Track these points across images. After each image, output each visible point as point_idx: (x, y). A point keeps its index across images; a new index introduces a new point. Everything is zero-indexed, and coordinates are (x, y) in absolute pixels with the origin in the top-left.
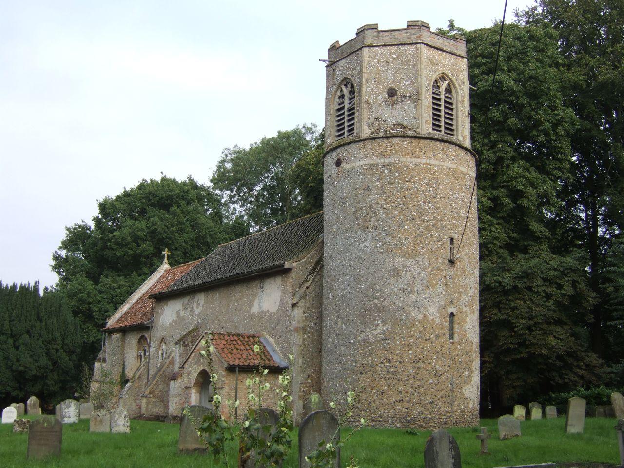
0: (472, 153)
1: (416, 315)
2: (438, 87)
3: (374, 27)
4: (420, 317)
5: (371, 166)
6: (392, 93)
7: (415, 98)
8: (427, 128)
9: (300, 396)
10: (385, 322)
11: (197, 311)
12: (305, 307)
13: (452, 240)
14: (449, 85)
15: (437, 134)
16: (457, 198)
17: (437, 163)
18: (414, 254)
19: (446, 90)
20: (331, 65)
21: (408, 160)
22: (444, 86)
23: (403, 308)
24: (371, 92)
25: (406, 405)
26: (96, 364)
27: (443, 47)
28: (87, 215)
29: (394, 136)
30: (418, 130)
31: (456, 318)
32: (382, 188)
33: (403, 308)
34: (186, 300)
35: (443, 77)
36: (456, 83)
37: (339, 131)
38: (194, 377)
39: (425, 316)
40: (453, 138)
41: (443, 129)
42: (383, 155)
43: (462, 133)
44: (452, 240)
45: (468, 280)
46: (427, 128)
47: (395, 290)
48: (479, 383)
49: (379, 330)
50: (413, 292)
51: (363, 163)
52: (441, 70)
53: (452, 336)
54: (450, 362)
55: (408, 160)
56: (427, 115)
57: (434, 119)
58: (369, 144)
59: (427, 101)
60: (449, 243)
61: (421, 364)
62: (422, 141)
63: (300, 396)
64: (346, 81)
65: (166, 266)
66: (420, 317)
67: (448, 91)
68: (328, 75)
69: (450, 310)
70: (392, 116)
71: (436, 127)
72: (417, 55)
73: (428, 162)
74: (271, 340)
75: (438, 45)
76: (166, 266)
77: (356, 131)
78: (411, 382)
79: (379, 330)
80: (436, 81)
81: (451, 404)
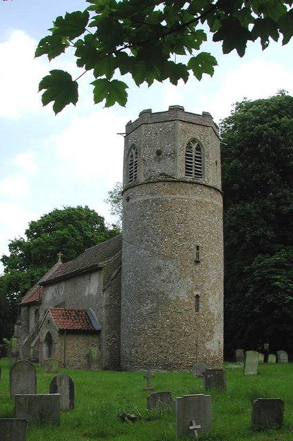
0: (221, 192)
1: (172, 296)
2: (191, 147)
3: (182, 109)
4: (174, 298)
5: (147, 201)
6: (159, 153)
7: (173, 155)
8: (181, 175)
9: (107, 349)
10: (152, 302)
11: (62, 293)
12: (111, 292)
13: (198, 248)
14: (198, 145)
15: (189, 179)
16: (202, 220)
17: (187, 197)
18: (170, 257)
19: (196, 148)
20: (127, 136)
21: (168, 197)
22: (194, 146)
23: (163, 292)
24: (147, 153)
25: (164, 354)
26: (15, 326)
27: (192, 121)
28: (20, 233)
29: (160, 181)
30: (174, 177)
31: (200, 298)
32: (152, 215)
33: (163, 292)
34: (56, 287)
35: (194, 140)
36: (203, 144)
37: (130, 178)
38: (43, 338)
39: (178, 298)
40: (200, 181)
41: (193, 175)
42: (152, 194)
43: (207, 176)
44: (198, 248)
45: (210, 273)
46: (181, 175)
47: (159, 281)
48: (222, 339)
49: (148, 307)
50: (170, 282)
51: (140, 199)
52: (191, 136)
53: (197, 310)
54: (195, 327)
55: (167, 196)
56: (181, 165)
57: (186, 169)
58: (144, 187)
59: (181, 156)
60: (195, 249)
61: (174, 328)
62: (177, 184)
63: (107, 349)
64: (133, 146)
65: (60, 263)
66: (174, 298)
67: (198, 149)
68: (125, 142)
69: (195, 293)
70: (158, 169)
71: (188, 173)
72: (175, 127)
73: (181, 197)
74: (94, 313)
75: (190, 120)
76: (60, 263)
77: (138, 178)
78: (168, 340)
79: (148, 307)
80: (189, 144)
81: (196, 354)
